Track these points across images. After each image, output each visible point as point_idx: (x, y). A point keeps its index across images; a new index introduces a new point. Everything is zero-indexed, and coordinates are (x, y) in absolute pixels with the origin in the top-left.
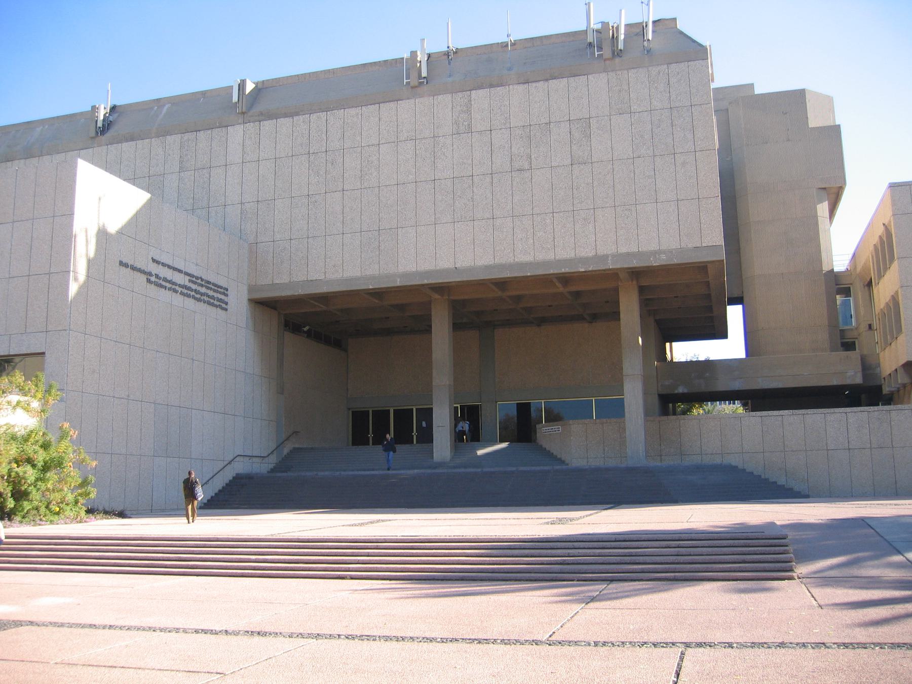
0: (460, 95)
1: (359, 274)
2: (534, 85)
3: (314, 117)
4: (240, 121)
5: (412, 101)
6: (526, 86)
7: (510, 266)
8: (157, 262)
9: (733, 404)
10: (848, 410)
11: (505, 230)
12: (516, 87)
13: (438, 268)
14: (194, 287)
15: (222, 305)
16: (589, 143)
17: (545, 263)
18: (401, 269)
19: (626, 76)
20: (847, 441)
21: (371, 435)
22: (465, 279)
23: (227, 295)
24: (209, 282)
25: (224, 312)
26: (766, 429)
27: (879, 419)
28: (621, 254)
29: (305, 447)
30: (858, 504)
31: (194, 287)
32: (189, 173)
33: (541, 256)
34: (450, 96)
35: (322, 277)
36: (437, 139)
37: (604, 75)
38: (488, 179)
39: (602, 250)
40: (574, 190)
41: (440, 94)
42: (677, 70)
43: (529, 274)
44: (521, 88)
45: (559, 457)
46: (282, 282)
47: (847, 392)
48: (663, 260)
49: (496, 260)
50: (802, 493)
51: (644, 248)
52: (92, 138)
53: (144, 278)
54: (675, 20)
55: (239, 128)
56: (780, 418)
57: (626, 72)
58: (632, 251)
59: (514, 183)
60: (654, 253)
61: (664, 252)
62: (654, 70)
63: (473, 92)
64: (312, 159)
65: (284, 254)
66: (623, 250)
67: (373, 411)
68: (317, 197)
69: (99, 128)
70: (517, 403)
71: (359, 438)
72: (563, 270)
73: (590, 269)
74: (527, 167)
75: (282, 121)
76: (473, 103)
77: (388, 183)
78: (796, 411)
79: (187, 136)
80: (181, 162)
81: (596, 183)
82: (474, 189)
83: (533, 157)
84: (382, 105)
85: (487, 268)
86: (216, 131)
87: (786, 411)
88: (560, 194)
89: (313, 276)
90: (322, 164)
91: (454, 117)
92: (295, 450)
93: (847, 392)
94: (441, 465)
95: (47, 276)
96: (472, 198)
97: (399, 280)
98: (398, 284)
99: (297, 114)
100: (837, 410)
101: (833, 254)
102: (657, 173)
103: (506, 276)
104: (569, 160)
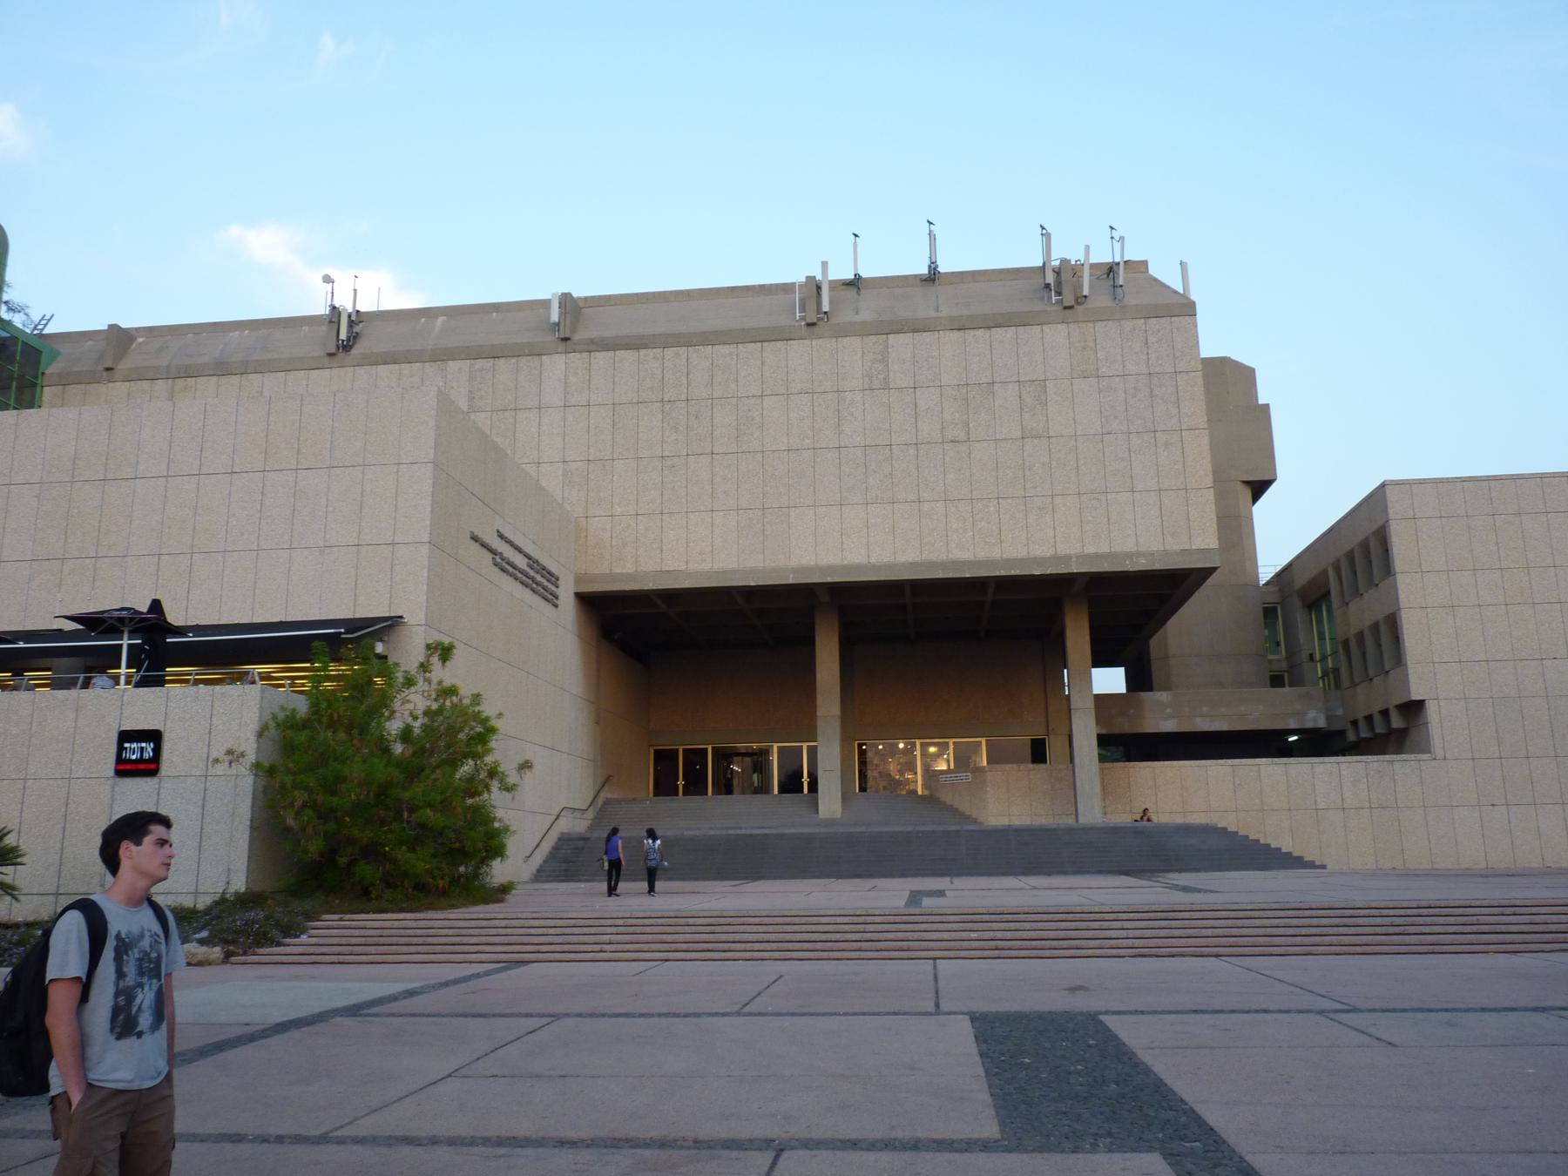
1: (735, 566)
2: (972, 332)
3: (669, 352)
4: (561, 348)
5: (807, 342)
6: (961, 333)
7: (943, 565)
8: (501, 536)
11: (935, 517)
12: (948, 333)
13: (845, 562)
14: (532, 573)
15: (552, 599)
17: (992, 563)
18: (795, 562)
19: (1092, 330)
20: (1340, 799)
21: (681, 783)
22: (882, 579)
23: (557, 587)
24: (544, 568)
25: (554, 609)
26: (1238, 782)
27: (1379, 771)
28: (1088, 555)
30: (1185, 889)
31: (532, 573)
32: (483, 415)
33: (982, 554)
34: (858, 339)
35: (683, 568)
36: (842, 394)
37: (1063, 326)
38: (912, 451)
39: (1063, 549)
40: (1027, 470)
41: (846, 336)
42: (1157, 326)
43: (968, 576)
44: (955, 335)
45: (967, 813)
46: (624, 571)
47: (1295, 738)
48: (1142, 564)
49: (924, 555)
51: (1117, 549)
52: (331, 355)
53: (489, 556)
54: (1145, 263)
55: (559, 360)
56: (1256, 768)
57: (1091, 325)
59: (947, 459)
60: (1130, 555)
62: (1128, 325)
63: (891, 336)
64: (668, 408)
65: (627, 534)
66: (1091, 549)
67: (684, 750)
68: (675, 460)
69: (343, 341)
71: (664, 787)
72: (1106, 565)
74: (963, 437)
75: (621, 354)
76: (890, 350)
77: (774, 448)
78: (1276, 759)
79: (480, 363)
80: (471, 398)
81: (1054, 463)
82: (894, 462)
83: (971, 425)
84: (765, 344)
85: (913, 565)
86: (524, 360)
89: (670, 565)
90: (681, 417)
92: (607, 802)
94: (831, 822)
95: (391, 547)
96: (891, 474)
97: (791, 576)
98: (791, 581)
99: (646, 347)
100: (1326, 759)
102: (1132, 455)
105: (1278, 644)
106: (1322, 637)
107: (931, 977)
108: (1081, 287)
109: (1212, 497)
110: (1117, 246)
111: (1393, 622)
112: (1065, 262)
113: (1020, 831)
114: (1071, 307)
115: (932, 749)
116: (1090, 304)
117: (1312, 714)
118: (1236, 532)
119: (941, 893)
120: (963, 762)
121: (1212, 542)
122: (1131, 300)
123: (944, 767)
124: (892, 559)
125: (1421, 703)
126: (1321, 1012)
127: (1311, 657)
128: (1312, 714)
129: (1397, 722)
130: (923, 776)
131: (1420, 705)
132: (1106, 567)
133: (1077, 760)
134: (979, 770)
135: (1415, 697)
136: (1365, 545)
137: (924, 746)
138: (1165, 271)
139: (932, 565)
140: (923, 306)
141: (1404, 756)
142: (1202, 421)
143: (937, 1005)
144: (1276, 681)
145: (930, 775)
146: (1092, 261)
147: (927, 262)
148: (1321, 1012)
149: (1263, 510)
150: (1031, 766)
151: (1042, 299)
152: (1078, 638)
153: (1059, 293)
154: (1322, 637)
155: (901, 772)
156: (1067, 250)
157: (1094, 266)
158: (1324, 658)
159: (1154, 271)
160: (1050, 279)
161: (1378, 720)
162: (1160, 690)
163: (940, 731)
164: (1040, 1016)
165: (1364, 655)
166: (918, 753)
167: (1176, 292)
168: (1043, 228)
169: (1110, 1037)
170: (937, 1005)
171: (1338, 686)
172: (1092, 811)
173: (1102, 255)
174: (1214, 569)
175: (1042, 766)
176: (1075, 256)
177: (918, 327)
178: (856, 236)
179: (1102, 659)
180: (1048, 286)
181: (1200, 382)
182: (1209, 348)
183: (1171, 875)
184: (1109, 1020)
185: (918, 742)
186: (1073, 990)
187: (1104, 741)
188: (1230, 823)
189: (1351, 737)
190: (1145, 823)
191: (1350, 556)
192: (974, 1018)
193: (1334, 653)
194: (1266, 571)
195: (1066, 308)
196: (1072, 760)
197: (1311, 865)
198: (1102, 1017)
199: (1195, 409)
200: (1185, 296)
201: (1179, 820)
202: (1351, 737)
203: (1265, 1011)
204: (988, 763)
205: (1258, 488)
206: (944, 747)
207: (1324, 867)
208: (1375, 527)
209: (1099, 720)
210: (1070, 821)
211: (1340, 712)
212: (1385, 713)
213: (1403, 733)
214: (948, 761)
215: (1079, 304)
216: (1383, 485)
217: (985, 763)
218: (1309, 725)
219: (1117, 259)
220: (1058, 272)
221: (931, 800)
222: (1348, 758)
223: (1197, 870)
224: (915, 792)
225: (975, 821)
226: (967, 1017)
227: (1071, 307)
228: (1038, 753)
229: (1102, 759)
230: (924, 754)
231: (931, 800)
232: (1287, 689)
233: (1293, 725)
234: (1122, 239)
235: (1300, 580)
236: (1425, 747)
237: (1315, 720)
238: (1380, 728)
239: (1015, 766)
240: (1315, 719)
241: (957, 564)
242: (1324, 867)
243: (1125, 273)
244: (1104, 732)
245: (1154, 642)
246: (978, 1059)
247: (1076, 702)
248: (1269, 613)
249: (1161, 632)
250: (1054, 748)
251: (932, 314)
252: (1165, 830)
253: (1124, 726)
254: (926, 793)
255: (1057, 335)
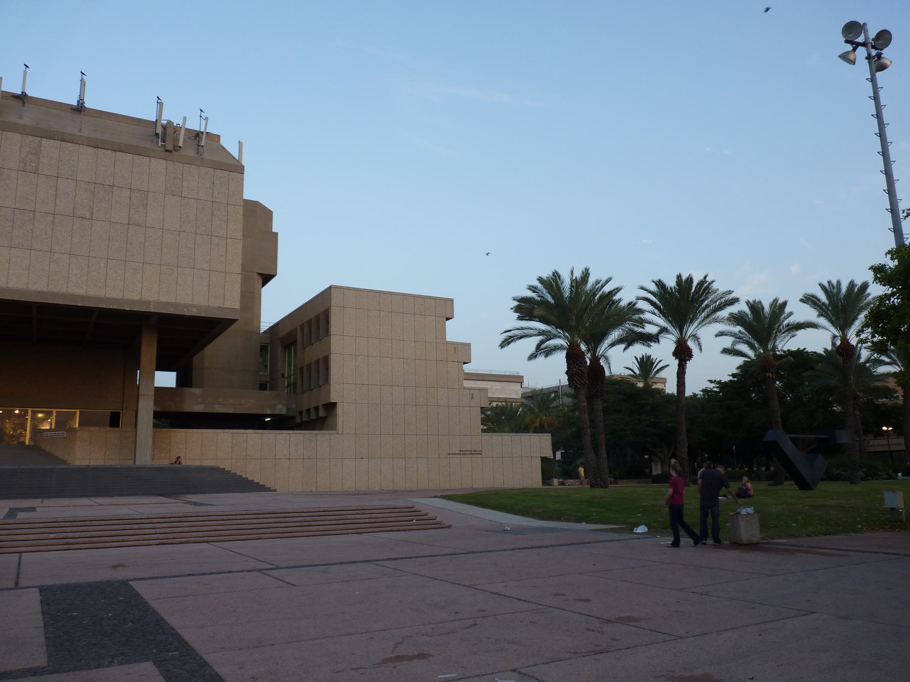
0: (31, 138)
2: (103, 151)
6: (95, 149)
7: (64, 296)
9: (482, 430)
10: (291, 432)
12: (86, 147)
16: (145, 211)
19: (181, 168)
29: (686, 449)
33: (92, 292)
38: (50, 218)
39: (146, 296)
43: (80, 305)
44: (91, 150)
45: (60, 457)
47: (269, 419)
48: (194, 312)
50: (272, 489)
54: (218, 136)
56: (245, 435)
57: (181, 164)
58: (171, 301)
60: (188, 306)
61: (195, 307)
62: (204, 170)
66: (164, 299)
70: (111, 412)
73: (135, 309)
74: (88, 215)
83: (94, 210)
87: (250, 430)
88: (115, 245)
91: (22, 156)
93: (269, 419)
100: (284, 432)
101: (261, 321)
102: (197, 247)
103: (58, 303)
104: (127, 220)
105: (266, 366)
106: (290, 365)
107: (16, 564)
108: (178, 140)
109: (239, 280)
110: (203, 122)
111: (326, 360)
112: (170, 122)
113: (95, 469)
114: (170, 151)
115: (40, 415)
116: (182, 152)
117: (279, 407)
118: (251, 302)
119: (33, 509)
120: (61, 424)
121: (237, 305)
122: (207, 156)
123: (48, 427)
124: (25, 287)
125: (335, 404)
126: (260, 571)
127: (283, 375)
128: (279, 407)
129: (322, 413)
130: (31, 433)
131: (335, 404)
132: (172, 311)
133: (139, 426)
134: (74, 430)
135: (332, 401)
136: (317, 318)
137: (34, 413)
138: (229, 144)
139: (55, 295)
140: (71, 126)
141: (323, 432)
142: (239, 233)
143: (17, 583)
144: (263, 387)
145: (36, 432)
146: (188, 126)
147: (77, 98)
148: (260, 571)
149: (268, 292)
150: (108, 428)
151: (153, 141)
152: (149, 352)
153: (164, 141)
154: (290, 365)
155: (15, 430)
156: (171, 115)
157: (187, 130)
158: (289, 377)
159: (223, 142)
160: (159, 130)
161: (312, 411)
162: (196, 387)
163: (47, 403)
164: (90, 585)
165: (310, 376)
166: (29, 417)
167: (234, 158)
168: (159, 98)
169: (799, 488)
170: (17, 583)
171: (295, 392)
172: (145, 457)
173: (194, 125)
174: (235, 321)
175: (116, 429)
176: (177, 121)
177: (63, 138)
178: (27, 66)
179: (163, 366)
180: (157, 135)
181: (241, 212)
182: (249, 194)
183: (188, 496)
184: (138, 586)
185: (30, 410)
186: (114, 567)
187: (157, 415)
188: (227, 466)
189: (298, 420)
190: (177, 465)
191: (310, 322)
192: (42, 589)
193: (295, 374)
194: (265, 325)
195: (167, 151)
196: (136, 426)
197: (268, 490)
198: (130, 583)
199: (236, 228)
200: (239, 161)
201: (198, 463)
202: (298, 420)
203: (230, 572)
204: (80, 425)
205: (266, 278)
206: (48, 415)
207: (275, 490)
208: (323, 309)
209: (156, 403)
210: (130, 463)
211: (294, 406)
212: (317, 408)
213: (324, 419)
214: (51, 423)
215: (175, 150)
216: (330, 287)
217: (77, 426)
218: (277, 412)
219: (202, 130)
220: (165, 128)
221: (35, 448)
222: (295, 432)
223: (204, 493)
224: (24, 443)
225: (65, 463)
226: (37, 590)
227: (170, 151)
228: (115, 421)
229: (155, 426)
230: (34, 418)
231: (35, 448)
232: (267, 392)
233: (268, 412)
234: (207, 119)
235: (282, 333)
236: (334, 428)
237: (281, 410)
238: (313, 417)
239: (97, 428)
240: (281, 409)
241: (73, 296)
242: (275, 490)
243: (206, 139)
244: (159, 410)
245: (196, 359)
246: (40, 616)
247: (142, 391)
248: (263, 349)
249: (203, 351)
250: (125, 418)
251: (78, 133)
252: (188, 469)
253: (172, 407)
254: (32, 443)
255: (159, 166)
